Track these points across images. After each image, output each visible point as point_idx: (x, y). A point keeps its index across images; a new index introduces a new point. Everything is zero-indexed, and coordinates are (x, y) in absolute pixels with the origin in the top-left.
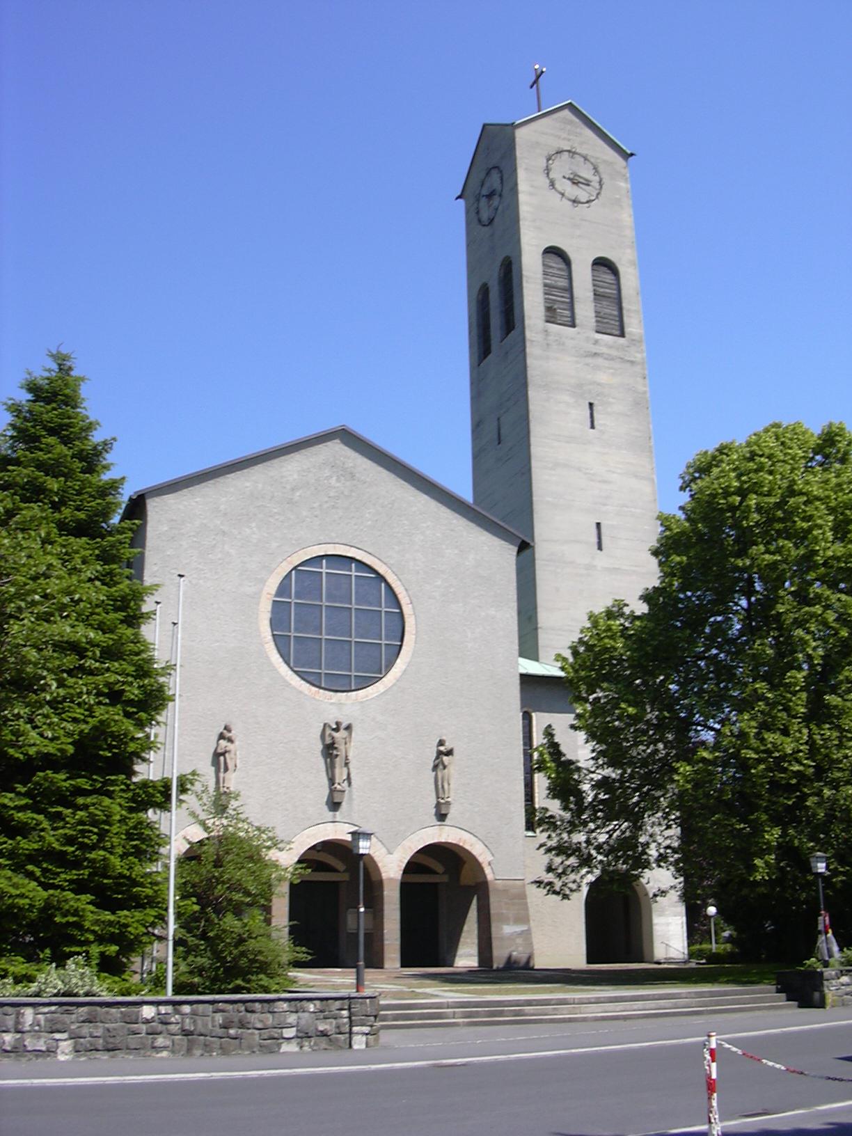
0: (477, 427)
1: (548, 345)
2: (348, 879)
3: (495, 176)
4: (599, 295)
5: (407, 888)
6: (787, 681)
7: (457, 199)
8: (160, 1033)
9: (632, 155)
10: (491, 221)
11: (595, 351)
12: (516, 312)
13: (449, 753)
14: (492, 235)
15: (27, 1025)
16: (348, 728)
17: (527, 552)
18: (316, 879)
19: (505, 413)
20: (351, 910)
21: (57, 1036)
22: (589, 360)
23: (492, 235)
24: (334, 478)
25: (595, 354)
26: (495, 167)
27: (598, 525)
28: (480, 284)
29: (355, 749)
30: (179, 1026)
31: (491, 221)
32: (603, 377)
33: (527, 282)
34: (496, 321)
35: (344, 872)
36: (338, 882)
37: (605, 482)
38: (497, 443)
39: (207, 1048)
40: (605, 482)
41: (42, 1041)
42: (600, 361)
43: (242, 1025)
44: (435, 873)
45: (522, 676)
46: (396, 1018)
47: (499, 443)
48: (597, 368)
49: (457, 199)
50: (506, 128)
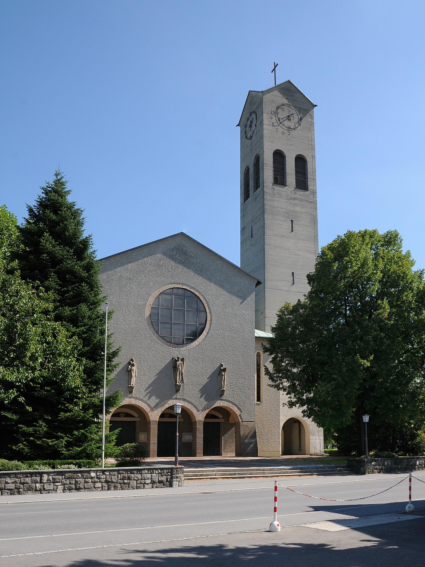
0: (243, 230)
1: (274, 194)
2: (183, 421)
3: (254, 116)
4: (298, 172)
5: (206, 425)
6: (30, 355)
7: (236, 126)
8: (97, 482)
9: (316, 106)
10: (251, 137)
11: (294, 197)
12: (261, 179)
13: (225, 370)
14: (252, 144)
15: (45, 480)
16: (183, 360)
17: (260, 286)
18: (118, 420)
19: (254, 224)
20: (184, 433)
21: (57, 484)
22: (292, 201)
23: (252, 144)
24: (178, 255)
25: (295, 198)
26: (253, 112)
27: (293, 273)
28: (246, 166)
29: (184, 368)
30: (105, 479)
31: (251, 137)
32: (298, 209)
33: (266, 166)
34: (252, 183)
35: (222, 418)
36: (135, 421)
37: (296, 255)
38: (251, 237)
39: (115, 488)
40: (296, 255)
41: (51, 486)
42: (297, 202)
43: (129, 478)
44: (134, 417)
45: (256, 337)
46: (235, 474)
47: (252, 238)
48: (295, 205)
49: (236, 126)
50: (259, 93)
